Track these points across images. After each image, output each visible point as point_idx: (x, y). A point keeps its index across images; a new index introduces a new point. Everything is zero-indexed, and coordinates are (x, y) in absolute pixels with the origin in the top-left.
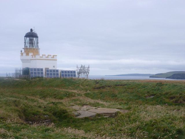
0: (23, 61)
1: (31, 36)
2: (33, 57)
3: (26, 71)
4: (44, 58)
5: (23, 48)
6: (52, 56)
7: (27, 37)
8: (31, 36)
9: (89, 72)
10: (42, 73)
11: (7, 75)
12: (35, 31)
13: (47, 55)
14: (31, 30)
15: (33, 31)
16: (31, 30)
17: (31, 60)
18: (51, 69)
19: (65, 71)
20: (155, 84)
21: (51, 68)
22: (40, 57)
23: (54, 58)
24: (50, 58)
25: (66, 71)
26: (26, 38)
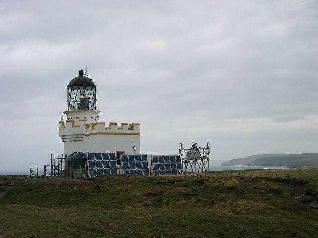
0: (65, 138)
1: (82, 83)
2: (88, 130)
3: (76, 161)
4: (114, 130)
5: (64, 112)
6: (107, 126)
7: (72, 89)
8: (82, 83)
9: (207, 158)
10: (146, 165)
11: (31, 170)
12: (89, 74)
13: (119, 125)
14: (81, 72)
15: (85, 76)
16: (81, 72)
17: (85, 137)
18: (92, 152)
19: (165, 157)
20: (63, 166)
21: (129, 152)
22: (106, 128)
23: (132, 130)
24: (125, 130)
25: (101, 154)
26: (70, 90)
